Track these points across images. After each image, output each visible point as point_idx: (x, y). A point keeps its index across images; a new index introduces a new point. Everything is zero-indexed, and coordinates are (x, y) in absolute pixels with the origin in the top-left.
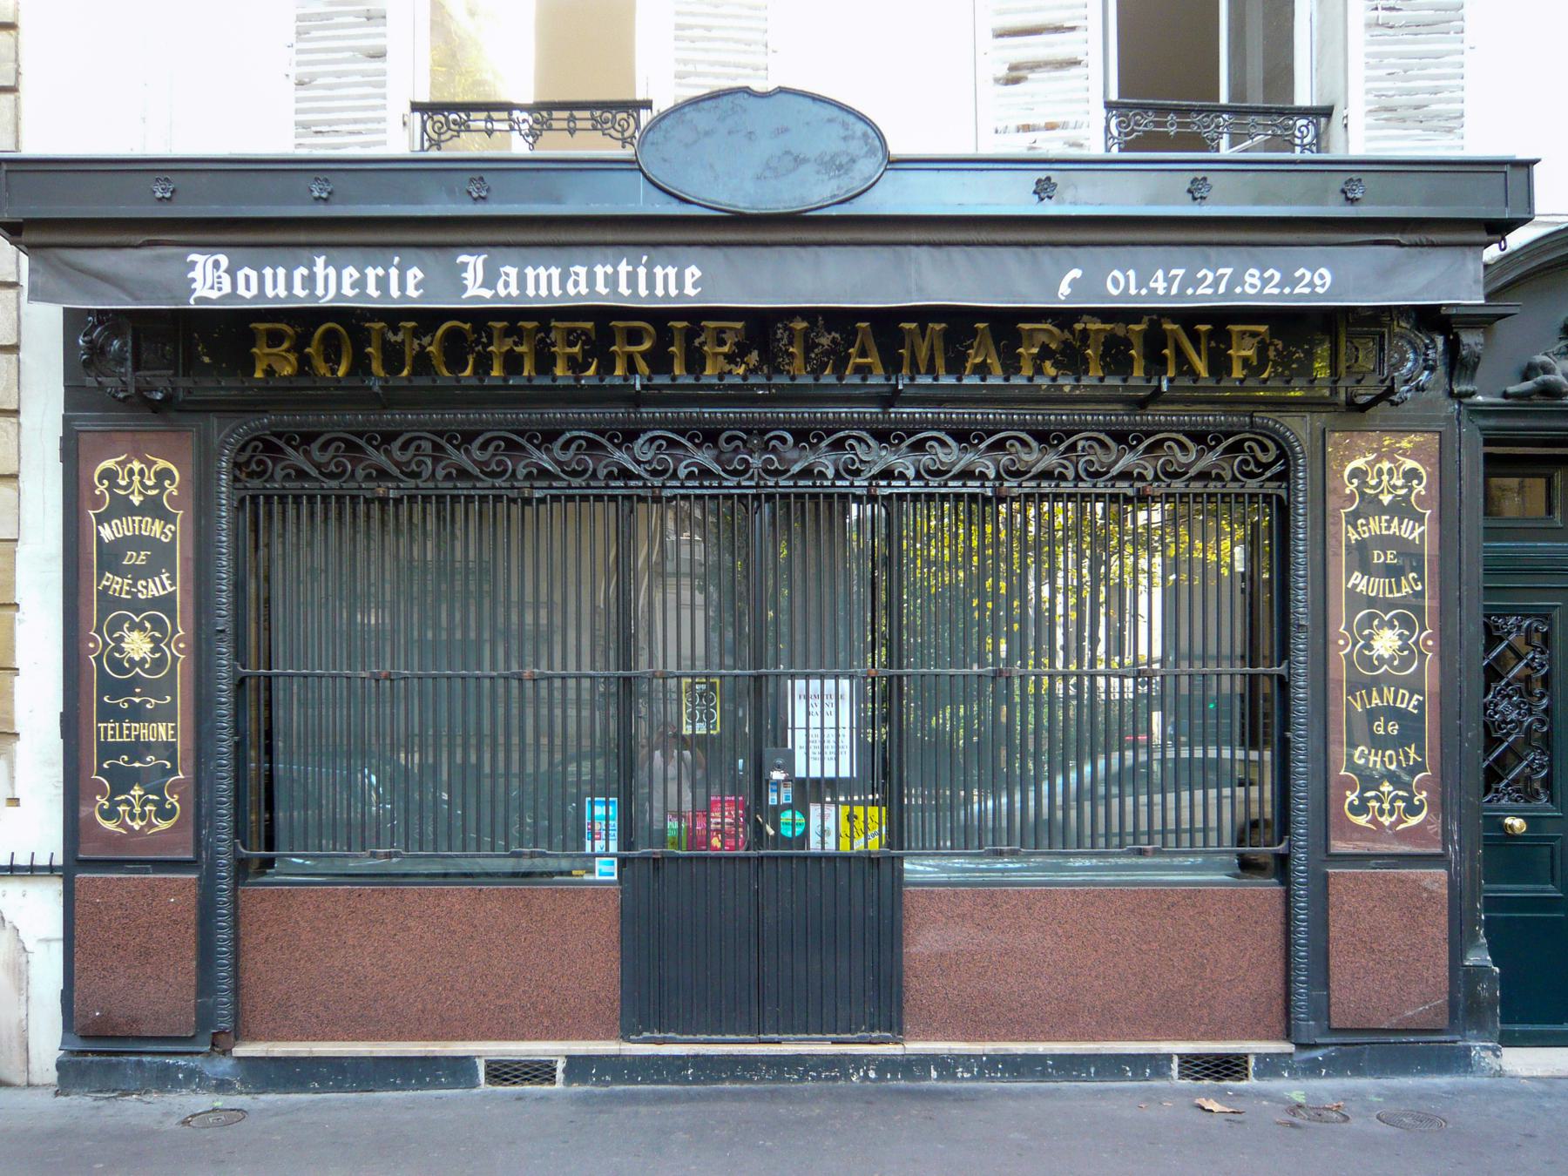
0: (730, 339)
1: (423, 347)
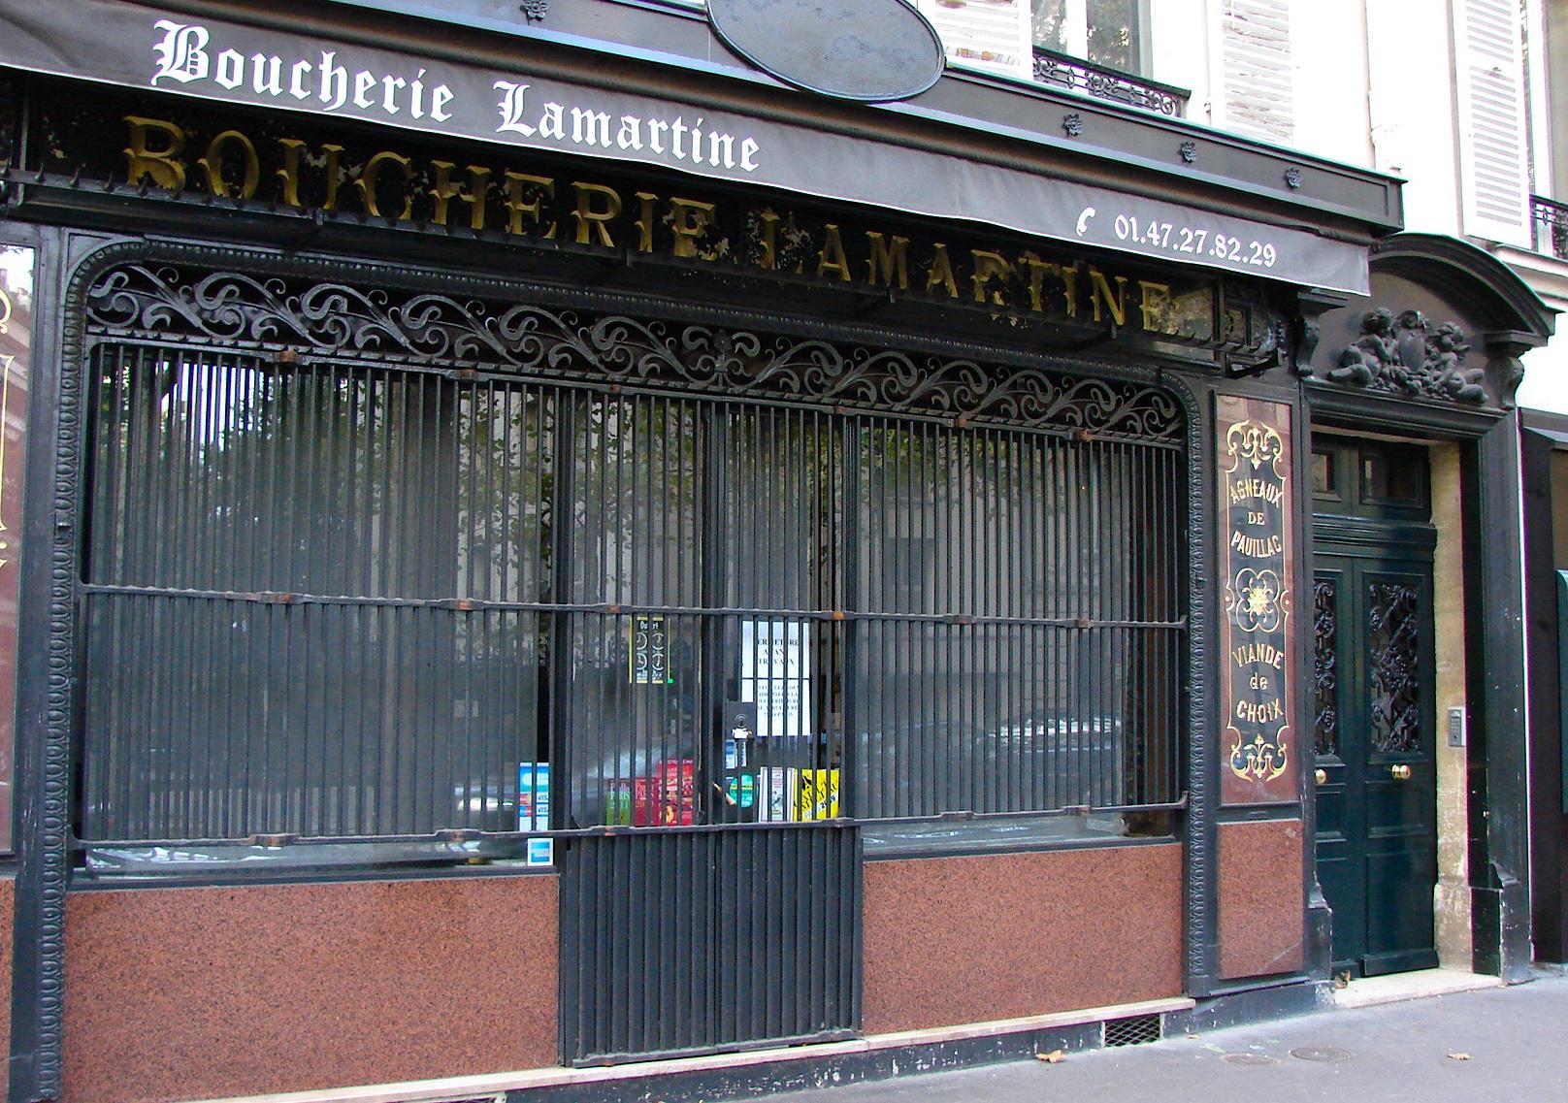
0: (701, 221)
1: (350, 179)
